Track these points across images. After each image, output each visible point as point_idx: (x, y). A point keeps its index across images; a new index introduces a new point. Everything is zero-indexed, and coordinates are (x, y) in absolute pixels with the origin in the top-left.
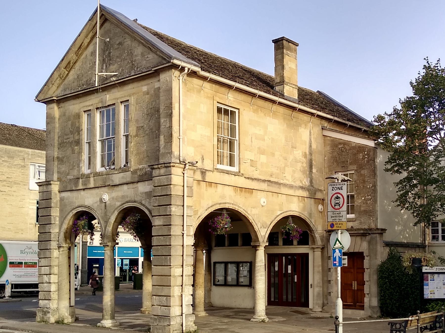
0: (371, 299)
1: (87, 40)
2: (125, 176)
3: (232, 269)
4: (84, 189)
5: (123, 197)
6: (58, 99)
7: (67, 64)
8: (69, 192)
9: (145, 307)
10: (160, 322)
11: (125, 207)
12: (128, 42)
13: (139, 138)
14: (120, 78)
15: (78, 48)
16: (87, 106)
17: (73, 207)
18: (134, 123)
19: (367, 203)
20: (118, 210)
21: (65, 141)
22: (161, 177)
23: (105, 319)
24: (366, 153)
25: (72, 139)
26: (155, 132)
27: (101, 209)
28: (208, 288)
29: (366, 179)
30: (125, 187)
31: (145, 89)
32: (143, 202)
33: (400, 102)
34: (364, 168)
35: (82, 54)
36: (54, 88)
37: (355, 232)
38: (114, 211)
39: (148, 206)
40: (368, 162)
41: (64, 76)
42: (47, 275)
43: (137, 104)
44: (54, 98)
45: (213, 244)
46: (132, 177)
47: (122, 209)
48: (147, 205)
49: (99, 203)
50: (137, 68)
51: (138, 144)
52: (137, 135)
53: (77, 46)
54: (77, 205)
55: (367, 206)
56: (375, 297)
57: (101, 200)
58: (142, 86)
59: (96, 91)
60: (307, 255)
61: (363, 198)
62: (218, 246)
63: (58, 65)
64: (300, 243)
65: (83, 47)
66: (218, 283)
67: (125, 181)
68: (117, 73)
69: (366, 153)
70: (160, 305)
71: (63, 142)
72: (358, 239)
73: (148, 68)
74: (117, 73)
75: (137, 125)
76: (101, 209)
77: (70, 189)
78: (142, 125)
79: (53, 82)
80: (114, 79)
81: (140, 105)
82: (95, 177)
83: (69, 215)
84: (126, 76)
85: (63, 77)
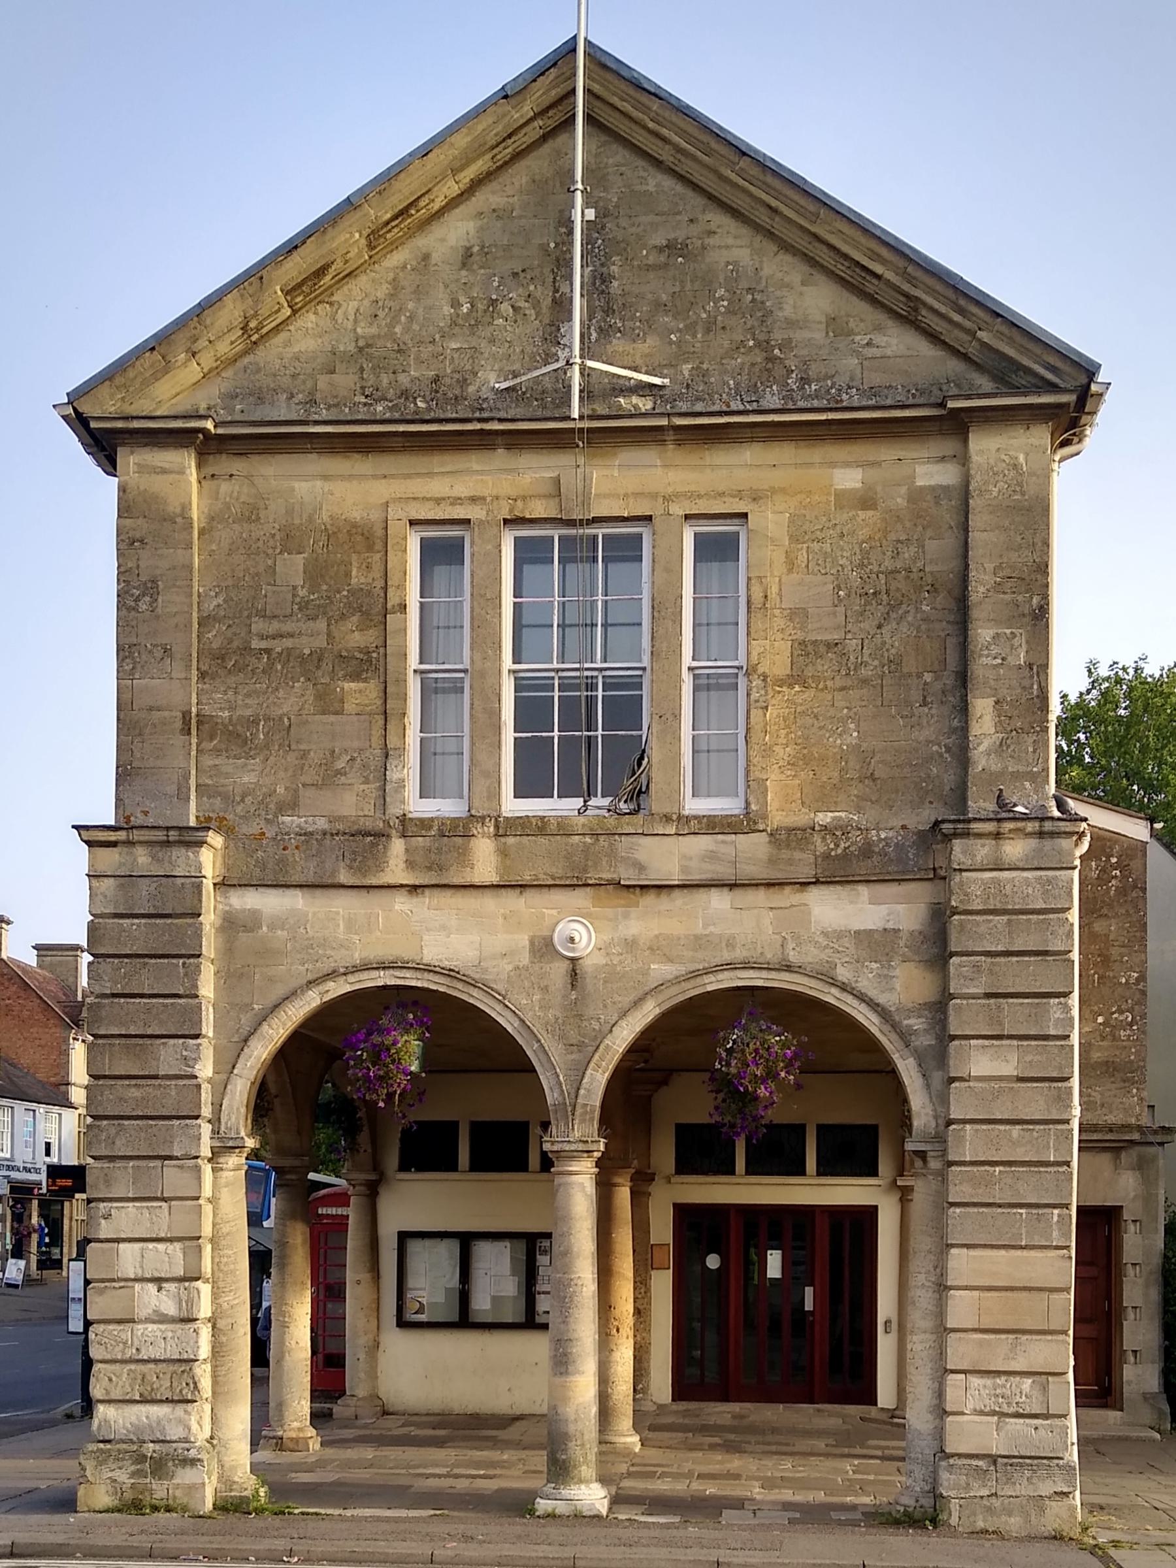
0: (1141, 1375)
1: (452, 188)
2: (723, 849)
3: (171, 1259)
4: (414, 889)
5: (699, 942)
6: (220, 431)
7: (302, 270)
8: (298, 892)
9: (295, 1424)
10: (1009, 1481)
11: (710, 988)
12: (732, 247)
13: (811, 693)
14: (699, 407)
15: (389, 211)
16: (438, 501)
17: (325, 967)
18: (779, 622)
19: (1115, 1038)
20: (661, 998)
21: (256, 644)
22: (1006, 874)
23: (581, 1481)
24: (1114, 860)
25: (321, 642)
26: (919, 676)
27: (545, 989)
28: (371, 1336)
29: (1115, 952)
30: (719, 901)
31: (849, 479)
32: (843, 974)
33: (1081, 694)
34: (1105, 911)
35: (395, 245)
36: (193, 371)
37: (1108, 1137)
38: (638, 1003)
39: (872, 993)
40: (1122, 892)
41: (264, 331)
42: (158, 1281)
43: (794, 539)
44: (209, 425)
45: (392, 1160)
46: (772, 861)
47: (681, 998)
48: (866, 985)
49: (525, 959)
50: (804, 381)
51: (809, 721)
52: (796, 678)
53: (397, 199)
54: (357, 957)
55: (1117, 1048)
56: (1153, 1363)
57: (544, 948)
58: (833, 465)
59: (559, 440)
60: (867, 1216)
61: (1100, 1020)
62: (421, 1169)
63: (263, 264)
64: (827, 1168)
65: (417, 215)
66: (423, 1318)
67: (724, 872)
68: (667, 381)
69: (1114, 860)
70: (993, 1413)
71: (246, 649)
72: (1105, 1159)
73: (873, 391)
74: (667, 381)
75: (800, 635)
76: (545, 989)
77: (311, 879)
78: (836, 636)
79: (202, 343)
80: (645, 404)
81: (816, 546)
82: (511, 840)
83: (298, 1003)
84: (723, 401)
85: (258, 330)
